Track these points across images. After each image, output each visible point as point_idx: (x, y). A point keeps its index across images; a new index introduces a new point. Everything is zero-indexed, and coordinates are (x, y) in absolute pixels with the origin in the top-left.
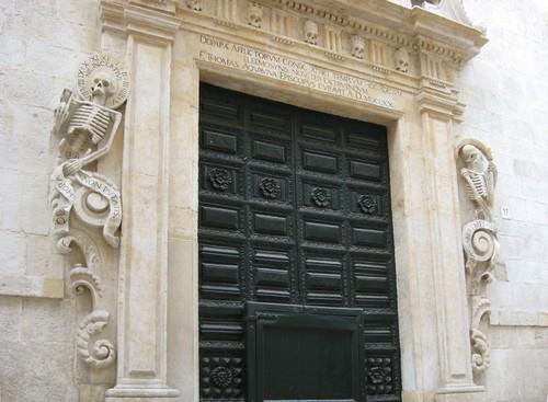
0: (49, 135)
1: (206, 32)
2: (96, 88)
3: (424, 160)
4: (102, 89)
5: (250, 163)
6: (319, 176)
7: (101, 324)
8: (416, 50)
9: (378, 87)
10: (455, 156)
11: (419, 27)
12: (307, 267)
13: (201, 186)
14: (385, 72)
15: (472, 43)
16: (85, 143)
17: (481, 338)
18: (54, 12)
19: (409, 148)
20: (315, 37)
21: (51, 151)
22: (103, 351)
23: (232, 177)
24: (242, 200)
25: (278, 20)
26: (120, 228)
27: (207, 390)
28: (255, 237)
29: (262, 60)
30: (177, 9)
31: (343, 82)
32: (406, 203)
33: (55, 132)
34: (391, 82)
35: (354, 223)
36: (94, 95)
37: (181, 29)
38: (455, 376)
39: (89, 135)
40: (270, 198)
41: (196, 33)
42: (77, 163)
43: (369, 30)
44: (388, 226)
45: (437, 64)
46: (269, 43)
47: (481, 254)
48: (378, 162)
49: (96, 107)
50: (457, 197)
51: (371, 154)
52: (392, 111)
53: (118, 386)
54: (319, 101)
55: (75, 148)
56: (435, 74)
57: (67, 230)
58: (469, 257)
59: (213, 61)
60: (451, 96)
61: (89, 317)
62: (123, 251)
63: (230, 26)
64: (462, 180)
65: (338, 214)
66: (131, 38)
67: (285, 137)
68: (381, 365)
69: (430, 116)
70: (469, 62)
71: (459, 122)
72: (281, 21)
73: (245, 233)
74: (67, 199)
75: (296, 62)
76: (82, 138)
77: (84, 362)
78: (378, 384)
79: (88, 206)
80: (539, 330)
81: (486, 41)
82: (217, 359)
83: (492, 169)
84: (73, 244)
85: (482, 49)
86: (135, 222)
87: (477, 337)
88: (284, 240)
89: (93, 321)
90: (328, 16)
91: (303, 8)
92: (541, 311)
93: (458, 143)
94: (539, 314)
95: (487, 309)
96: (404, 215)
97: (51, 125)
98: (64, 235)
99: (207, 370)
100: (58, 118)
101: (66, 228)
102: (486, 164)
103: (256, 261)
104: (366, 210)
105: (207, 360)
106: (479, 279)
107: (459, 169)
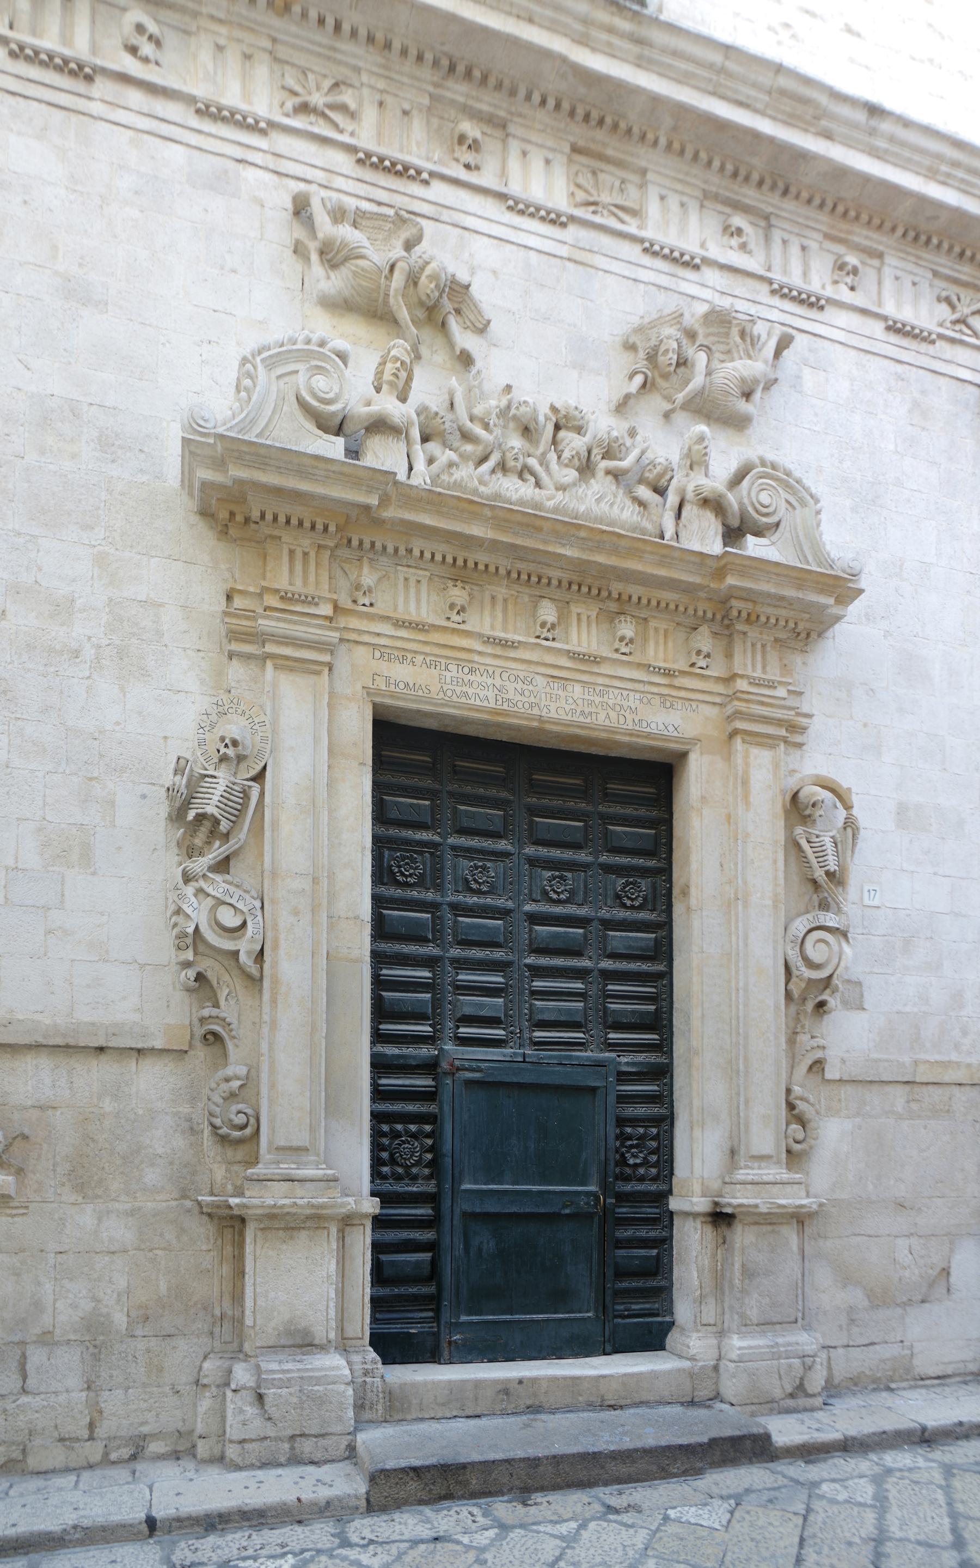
0: (162, 824)
1: (383, 641)
2: (223, 750)
3: (729, 817)
4: (231, 752)
5: (451, 840)
6: (556, 853)
7: (239, 1083)
8: (728, 627)
9: (657, 701)
10: (784, 806)
11: (732, 587)
12: (533, 993)
13: (374, 883)
14: (668, 673)
15: (831, 601)
16: (211, 832)
17: (807, 1101)
18: (159, 634)
19: (703, 799)
20: (553, 626)
21: (167, 848)
22: (241, 1119)
23: (422, 865)
24: (439, 899)
25: (406, 587)
26: (262, 949)
27: (385, 1169)
28: (455, 952)
29: (466, 678)
30: (336, 608)
31: (597, 699)
32: (693, 891)
33: (170, 818)
34: (680, 688)
35: (608, 924)
36: (221, 760)
37: (341, 640)
38: (754, 1158)
39: (217, 822)
40: (479, 892)
41: (366, 644)
42: (201, 864)
43: (644, 601)
44: (666, 925)
45: (763, 646)
46: (478, 646)
47: (817, 967)
48: (652, 823)
49: (223, 778)
50: (781, 875)
51: (642, 812)
52: (677, 740)
53: (260, 1166)
54: (558, 735)
55: (198, 841)
56: (759, 666)
57: (191, 958)
58: (795, 972)
59: (392, 688)
60: (789, 703)
61: (221, 1074)
62: (266, 984)
63: (418, 627)
64: (794, 846)
65: (583, 911)
66: (269, 664)
67: (504, 795)
68: (642, 1138)
69: (744, 741)
70: (829, 634)
71: (800, 745)
72: (499, 607)
73: (443, 949)
74: (188, 916)
75: (522, 674)
76: (207, 824)
77: (217, 1134)
78: (636, 1165)
79: (218, 924)
80: (916, 1089)
81: (861, 591)
82: (399, 1127)
83: (850, 824)
84: (200, 977)
85: (851, 608)
86: (283, 944)
87: (797, 1098)
88: (499, 954)
89: (227, 1080)
90: (575, 587)
91: (534, 579)
92: (923, 1056)
93: (792, 783)
94: (916, 1063)
95: (819, 1054)
96: (688, 908)
97: (164, 810)
98: (187, 965)
99: (385, 1141)
100: (171, 799)
101: (190, 955)
102: (841, 814)
103: (458, 987)
104: (629, 903)
105: (385, 1128)
106: (810, 1006)
107: (789, 828)
